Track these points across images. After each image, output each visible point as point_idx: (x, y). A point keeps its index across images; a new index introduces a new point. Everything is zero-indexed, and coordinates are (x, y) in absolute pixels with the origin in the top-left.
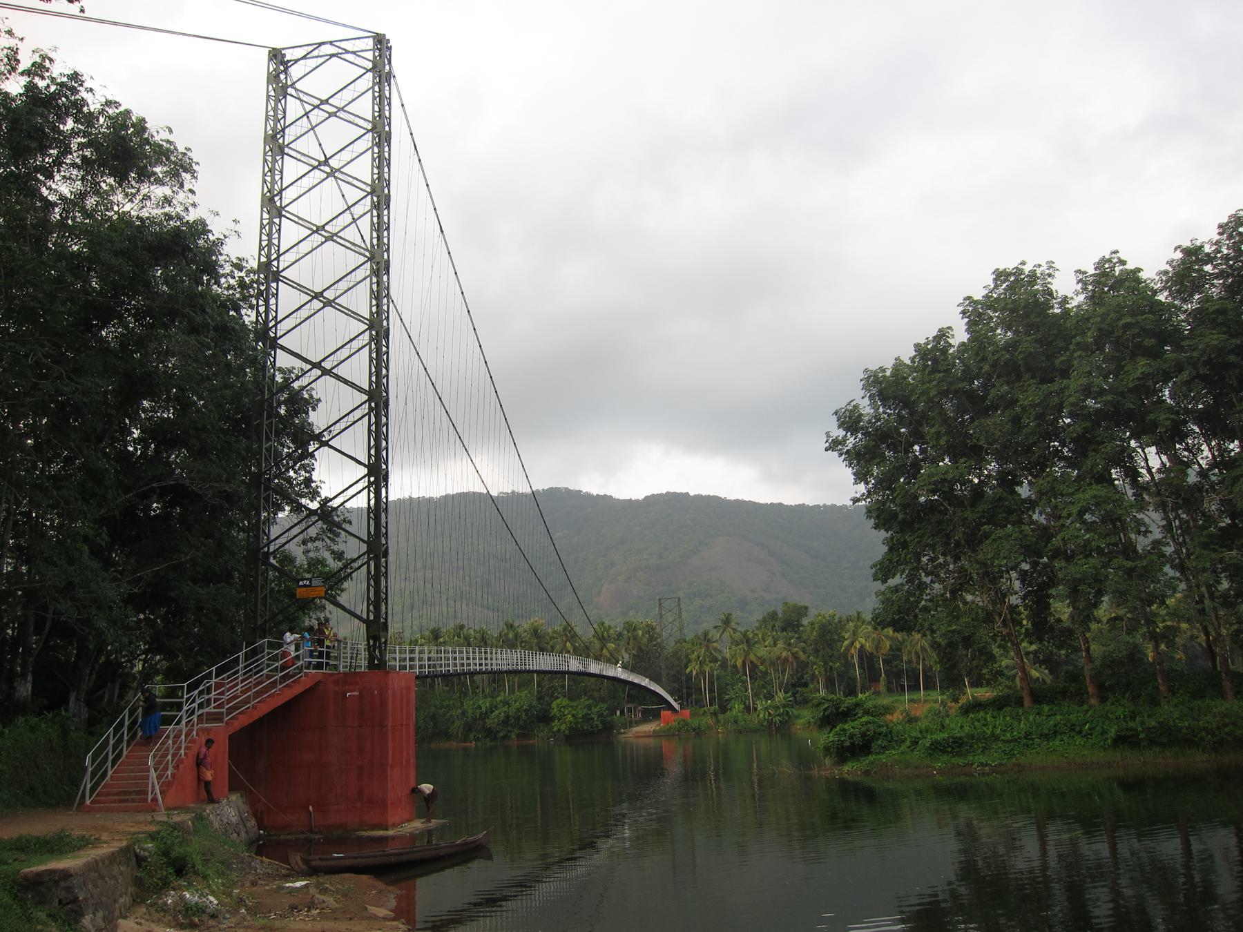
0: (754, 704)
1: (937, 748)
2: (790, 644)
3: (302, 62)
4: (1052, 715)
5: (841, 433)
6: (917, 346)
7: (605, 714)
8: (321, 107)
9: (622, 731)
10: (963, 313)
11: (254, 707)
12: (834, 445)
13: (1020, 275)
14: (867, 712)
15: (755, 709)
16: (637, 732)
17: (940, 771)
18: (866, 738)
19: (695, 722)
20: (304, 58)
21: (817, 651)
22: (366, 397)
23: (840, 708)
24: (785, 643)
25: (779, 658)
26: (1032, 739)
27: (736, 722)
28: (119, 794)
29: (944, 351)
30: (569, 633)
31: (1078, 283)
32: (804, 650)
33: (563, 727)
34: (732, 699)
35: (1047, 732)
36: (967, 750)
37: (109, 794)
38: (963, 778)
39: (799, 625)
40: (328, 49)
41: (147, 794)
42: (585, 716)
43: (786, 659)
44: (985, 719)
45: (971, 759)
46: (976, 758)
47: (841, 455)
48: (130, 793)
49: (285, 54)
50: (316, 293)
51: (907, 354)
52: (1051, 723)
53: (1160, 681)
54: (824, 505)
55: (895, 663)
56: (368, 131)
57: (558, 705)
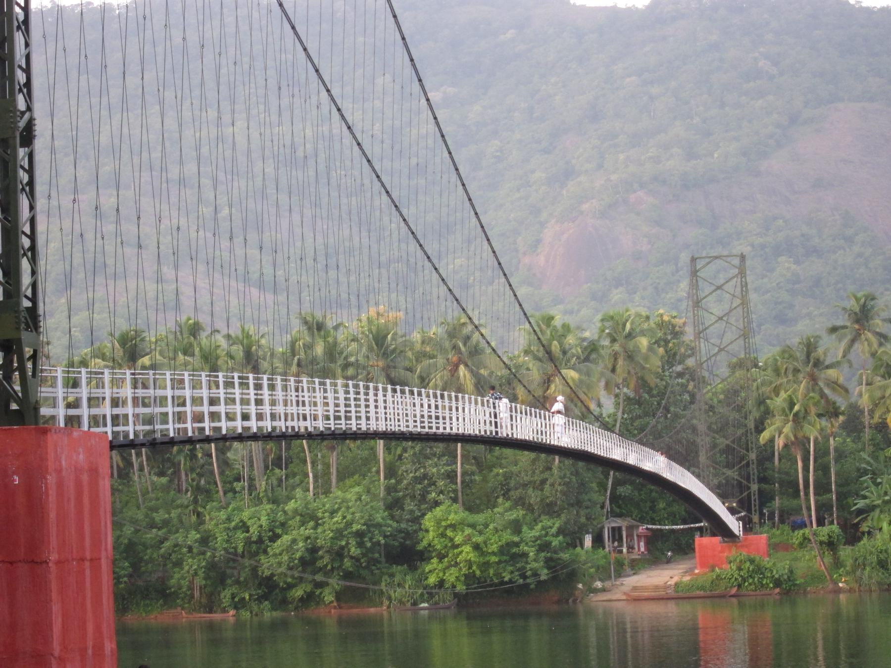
9: (599, 584)
16: (635, 588)
19: (779, 565)
33: (451, 576)
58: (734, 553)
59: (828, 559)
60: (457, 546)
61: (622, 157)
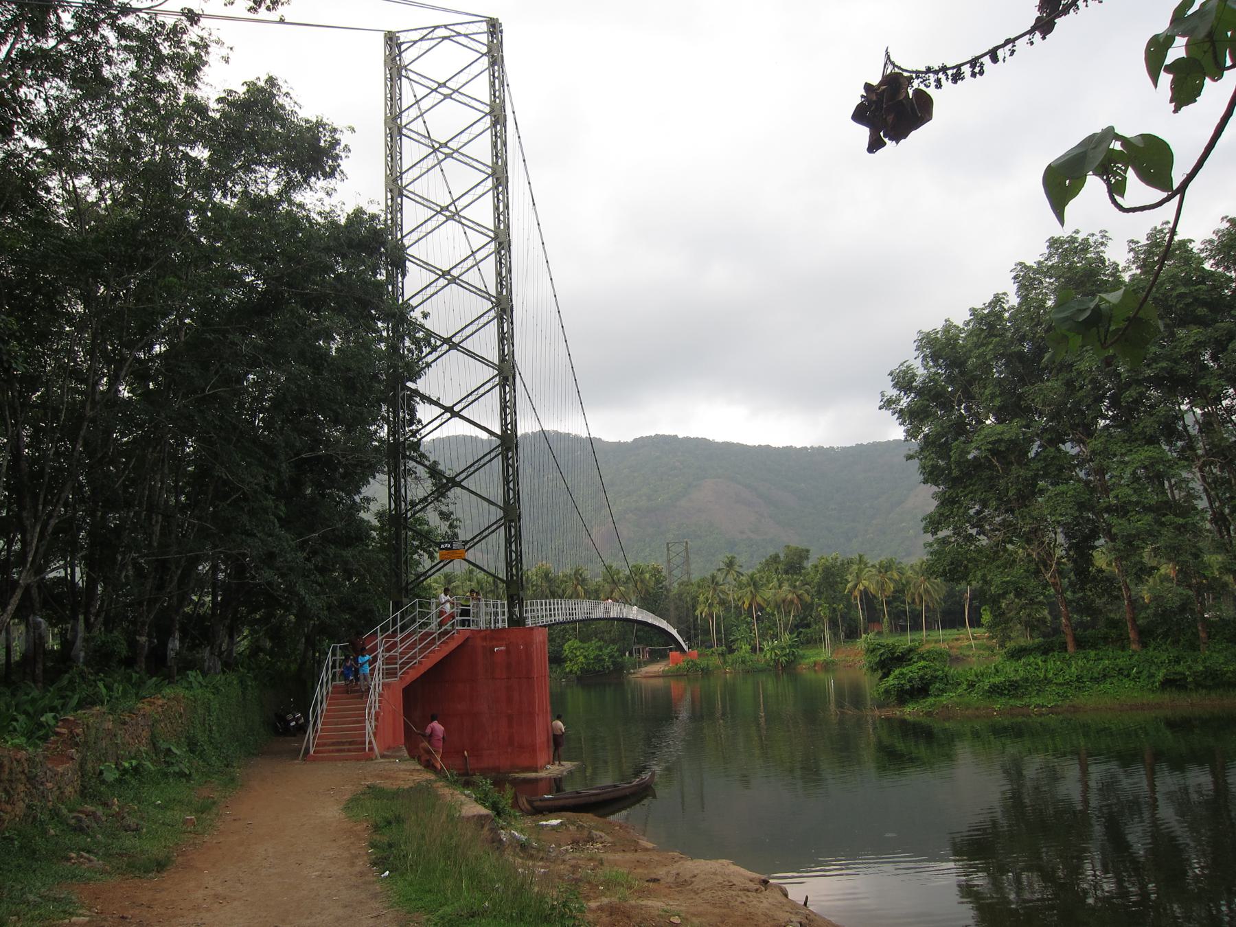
0: (760, 644)
1: (994, 690)
2: (795, 587)
3: (420, 43)
4: (1099, 659)
5: (895, 392)
6: (973, 311)
7: (616, 655)
8: (451, 92)
9: (632, 671)
10: (1015, 278)
11: (420, 663)
12: (888, 404)
13: (1073, 243)
14: (922, 657)
15: (761, 650)
16: (647, 672)
17: (1000, 713)
18: (924, 682)
19: (703, 662)
20: (421, 39)
21: (819, 593)
22: (496, 372)
23: (895, 653)
24: (790, 585)
25: (784, 601)
26: (1083, 682)
27: (743, 662)
28: (333, 744)
29: (999, 316)
30: (578, 577)
31: (1129, 252)
32: (807, 592)
33: (575, 668)
34: (738, 639)
35: (1096, 675)
36: (1023, 692)
37: (325, 745)
38: (1020, 719)
39: (801, 567)
40: (442, 32)
41: (365, 743)
42: (595, 658)
43: (792, 601)
44: (1037, 664)
45: (1028, 700)
46: (1033, 700)
47: (894, 414)
48: (343, 743)
49: (399, 37)
50: (443, 272)
51: (961, 318)
52: (1100, 667)
53: (1200, 628)
54: (812, 447)
55: (895, 604)
56: (486, 114)
57: (570, 648)
58: (685, 658)
59: (722, 660)
60: (577, 657)
61: (623, 500)
